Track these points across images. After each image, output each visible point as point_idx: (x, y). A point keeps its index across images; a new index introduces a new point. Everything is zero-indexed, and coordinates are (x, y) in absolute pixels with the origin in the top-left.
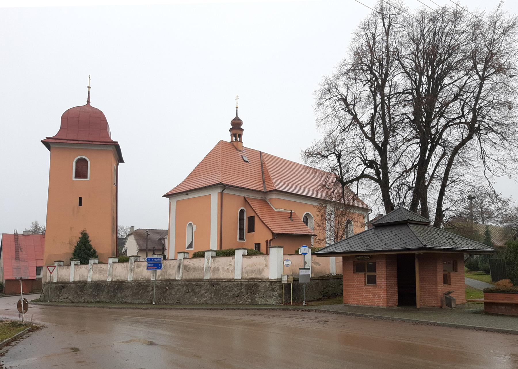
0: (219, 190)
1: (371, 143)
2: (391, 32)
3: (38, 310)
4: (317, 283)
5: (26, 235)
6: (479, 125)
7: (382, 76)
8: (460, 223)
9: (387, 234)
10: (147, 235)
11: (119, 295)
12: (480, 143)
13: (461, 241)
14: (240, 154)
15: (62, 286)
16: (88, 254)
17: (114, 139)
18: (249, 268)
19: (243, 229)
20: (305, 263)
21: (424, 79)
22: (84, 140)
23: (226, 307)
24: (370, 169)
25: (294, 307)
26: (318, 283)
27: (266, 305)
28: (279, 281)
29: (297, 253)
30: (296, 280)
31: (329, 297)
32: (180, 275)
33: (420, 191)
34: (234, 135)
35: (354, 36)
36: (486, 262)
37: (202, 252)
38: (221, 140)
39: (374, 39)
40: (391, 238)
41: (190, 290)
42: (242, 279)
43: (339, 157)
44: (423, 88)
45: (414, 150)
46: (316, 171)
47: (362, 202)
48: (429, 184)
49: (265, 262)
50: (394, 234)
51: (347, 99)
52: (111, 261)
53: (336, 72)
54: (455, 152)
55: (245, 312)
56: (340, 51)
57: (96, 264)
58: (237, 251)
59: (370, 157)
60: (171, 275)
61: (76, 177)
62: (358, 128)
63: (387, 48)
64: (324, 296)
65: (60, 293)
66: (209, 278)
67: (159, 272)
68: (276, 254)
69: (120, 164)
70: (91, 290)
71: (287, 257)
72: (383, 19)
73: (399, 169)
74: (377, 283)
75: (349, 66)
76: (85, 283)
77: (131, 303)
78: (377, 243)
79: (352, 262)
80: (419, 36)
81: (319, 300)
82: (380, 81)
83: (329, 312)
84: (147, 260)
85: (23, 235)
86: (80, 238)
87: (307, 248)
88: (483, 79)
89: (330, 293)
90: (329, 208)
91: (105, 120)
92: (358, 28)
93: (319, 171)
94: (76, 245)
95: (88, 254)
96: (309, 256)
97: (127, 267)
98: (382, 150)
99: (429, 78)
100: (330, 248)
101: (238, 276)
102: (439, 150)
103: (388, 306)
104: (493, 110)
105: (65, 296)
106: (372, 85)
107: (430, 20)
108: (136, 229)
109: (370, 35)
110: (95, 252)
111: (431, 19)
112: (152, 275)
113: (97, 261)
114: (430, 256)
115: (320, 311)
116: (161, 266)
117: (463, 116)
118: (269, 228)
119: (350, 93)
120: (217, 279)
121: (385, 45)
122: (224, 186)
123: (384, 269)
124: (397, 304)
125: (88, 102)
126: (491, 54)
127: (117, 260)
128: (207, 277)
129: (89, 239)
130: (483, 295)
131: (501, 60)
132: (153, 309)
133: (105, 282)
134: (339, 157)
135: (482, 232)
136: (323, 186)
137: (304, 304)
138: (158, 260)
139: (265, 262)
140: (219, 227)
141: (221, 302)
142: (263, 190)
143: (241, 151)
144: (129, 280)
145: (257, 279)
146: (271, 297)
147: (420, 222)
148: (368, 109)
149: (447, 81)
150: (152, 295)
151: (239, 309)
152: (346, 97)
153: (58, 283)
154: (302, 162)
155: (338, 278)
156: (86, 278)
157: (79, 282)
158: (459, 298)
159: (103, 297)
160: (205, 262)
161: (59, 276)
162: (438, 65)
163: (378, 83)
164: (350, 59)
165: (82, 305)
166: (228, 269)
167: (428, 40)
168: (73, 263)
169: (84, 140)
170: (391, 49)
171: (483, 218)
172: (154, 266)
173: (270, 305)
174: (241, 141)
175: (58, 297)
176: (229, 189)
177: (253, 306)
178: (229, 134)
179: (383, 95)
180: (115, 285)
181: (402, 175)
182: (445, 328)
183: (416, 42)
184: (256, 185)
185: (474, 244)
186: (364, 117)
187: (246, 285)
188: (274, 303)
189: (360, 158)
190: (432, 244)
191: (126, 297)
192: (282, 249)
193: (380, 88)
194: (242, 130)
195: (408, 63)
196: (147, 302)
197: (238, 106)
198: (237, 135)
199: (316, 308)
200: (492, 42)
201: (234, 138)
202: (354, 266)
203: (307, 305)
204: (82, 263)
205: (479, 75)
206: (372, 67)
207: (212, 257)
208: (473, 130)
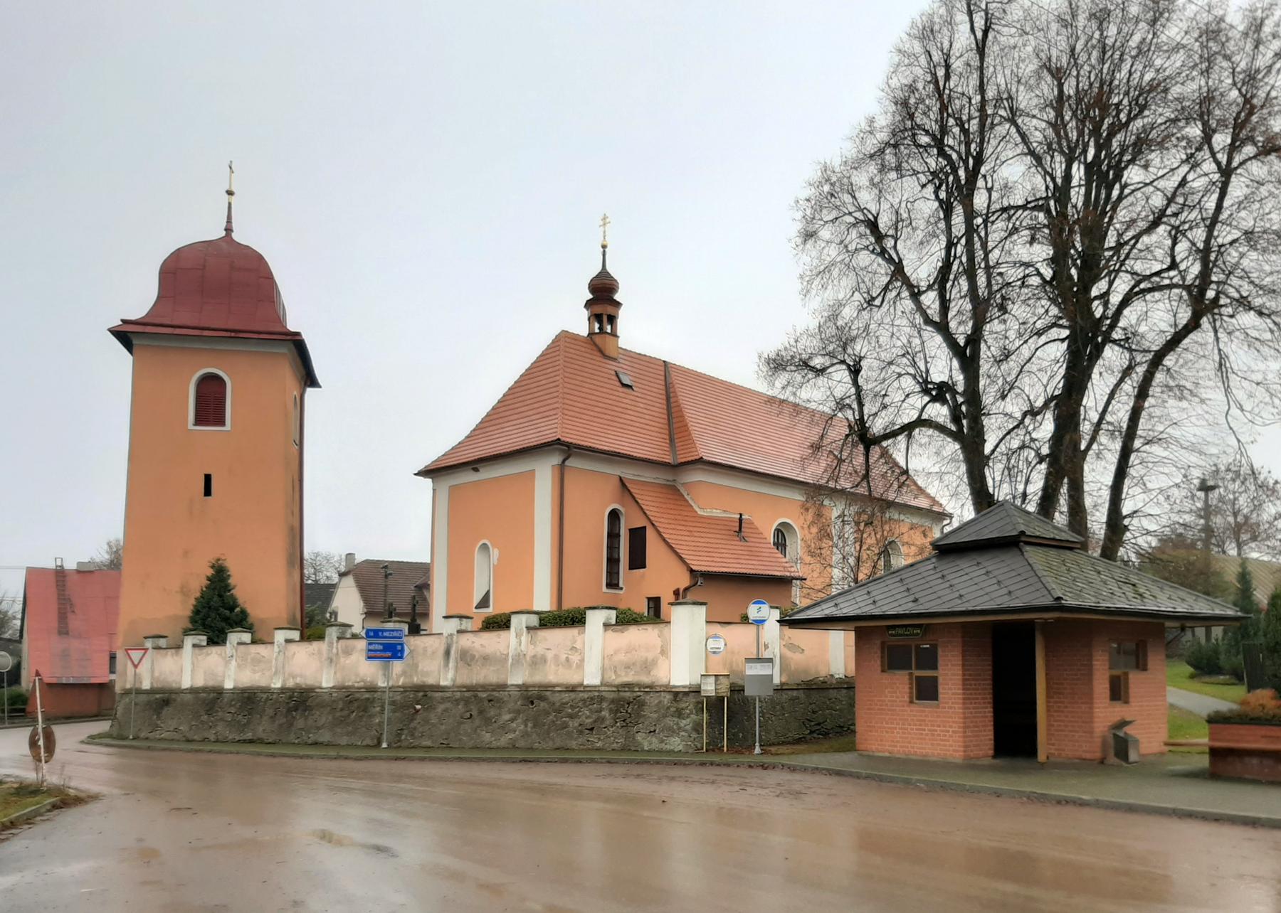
0: (556, 460)
1: (938, 339)
2: (992, 49)
3: (104, 759)
4: (793, 699)
5: (84, 572)
6: (1218, 293)
7: (966, 162)
8: (1182, 553)
9: (967, 571)
10: (386, 576)
11: (300, 723)
12: (1217, 339)
13: (1156, 591)
14: (612, 366)
15: (163, 700)
16: (226, 619)
17: (292, 326)
18: (622, 657)
19: (618, 560)
20: (765, 648)
21: (1078, 172)
22: (217, 327)
23: (563, 756)
24: (938, 405)
25: (731, 759)
26: (798, 698)
27: (661, 752)
28: (696, 691)
29: (745, 620)
30: (737, 690)
31: (826, 734)
32: (451, 674)
33: (1065, 460)
34: (598, 317)
35: (896, 59)
36: (1238, 653)
37: (500, 615)
38: (564, 332)
39: (948, 67)
40: (976, 580)
41: (474, 713)
42: (602, 684)
43: (855, 371)
44: (1077, 196)
45: (1054, 352)
46: (797, 409)
47: (921, 491)
48: (1089, 447)
49: (658, 642)
50: (984, 571)
51: (879, 221)
52: (280, 636)
53: (850, 150)
54: (1157, 361)
55: (605, 769)
56: (854, 95)
58: (589, 614)
59: (938, 376)
61: (199, 421)
62: (905, 294)
63: (982, 89)
64: (812, 732)
65: (158, 718)
66: (520, 682)
67: (397, 666)
68: (687, 623)
69: (309, 391)
71: (718, 629)
72: (970, 13)
73: (1015, 407)
74: (940, 696)
75: (883, 136)
76: (218, 692)
77: (328, 745)
78: (940, 594)
79: (878, 642)
80: (1064, 61)
81: (798, 741)
82: (962, 173)
83: (816, 770)
84: (368, 636)
85: (78, 572)
86: (208, 579)
87: (765, 608)
88: (1226, 172)
89: (829, 725)
90: (835, 510)
91: (269, 277)
92: (905, 37)
93: (806, 409)
94: (198, 595)
95: (226, 619)
96: (772, 629)
97: (320, 652)
98: (967, 355)
99: (1089, 167)
100: (824, 606)
101: (592, 677)
102: (1113, 356)
103: (967, 758)
104: (1253, 255)
105: (171, 723)
106: (940, 185)
107: (1092, 16)
108: (359, 558)
109: (937, 56)
110: (244, 614)
111: (1094, 14)
112: (381, 673)
113: (246, 637)
114: (1075, 628)
115: (793, 769)
116: (402, 651)
117: (1174, 265)
118: (681, 558)
119: (885, 206)
120: (540, 686)
121: (974, 80)
122: (567, 449)
123: (958, 660)
124: (991, 752)
125: (229, 230)
126: (1248, 105)
127: (203, 639)
128: (517, 678)
129: (231, 581)
130: (1206, 729)
131: (1272, 122)
132: (381, 759)
133: (266, 690)
134: (855, 371)
135: (1231, 574)
136: (816, 447)
137: (757, 750)
138: (395, 634)
140: (557, 554)
141: (550, 744)
142: (669, 459)
143: (614, 359)
144: (324, 685)
145: (639, 685)
147: (1054, 539)
148: (933, 250)
149: (1133, 175)
150: (381, 724)
151: (592, 761)
152: (876, 218)
154: (761, 387)
155: (847, 685)
157: (204, 689)
158: (1149, 739)
159: (263, 728)
160: (512, 641)
161: (156, 674)
162: (1112, 133)
163: (957, 178)
164: (885, 117)
165: (209, 748)
166: (567, 660)
167: (1087, 68)
168: (189, 641)
170: (991, 93)
171: (1237, 541)
173: (670, 752)
174: (614, 334)
175: (155, 727)
177: (630, 756)
178: (585, 314)
179: (970, 214)
180: (291, 697)
181: (1022, 422)
182: (1101, 812)
183: (1058, 75)
184: (649, 444)
185: (1190, 599)
186: (922, 268)
187: (613, 701)
188: (681, 747)
189: (914, 377)
190: (1078, 596)
191: (318, 728)
192: (703, 608)
193: (966, 192)
194: (618, 304)
195: (1038, 129)
196: (368, 741)
197: (609, 242)
198: (605, 318)
199: (784, 760)
200: (1251, 78)
201: (597, 326)
202: (882, 652)
203: (764, 752)
204: (213, 642)
205: (1218, 163)
206: (942, 140)
207: (529, 628)
208: (1202, 305)
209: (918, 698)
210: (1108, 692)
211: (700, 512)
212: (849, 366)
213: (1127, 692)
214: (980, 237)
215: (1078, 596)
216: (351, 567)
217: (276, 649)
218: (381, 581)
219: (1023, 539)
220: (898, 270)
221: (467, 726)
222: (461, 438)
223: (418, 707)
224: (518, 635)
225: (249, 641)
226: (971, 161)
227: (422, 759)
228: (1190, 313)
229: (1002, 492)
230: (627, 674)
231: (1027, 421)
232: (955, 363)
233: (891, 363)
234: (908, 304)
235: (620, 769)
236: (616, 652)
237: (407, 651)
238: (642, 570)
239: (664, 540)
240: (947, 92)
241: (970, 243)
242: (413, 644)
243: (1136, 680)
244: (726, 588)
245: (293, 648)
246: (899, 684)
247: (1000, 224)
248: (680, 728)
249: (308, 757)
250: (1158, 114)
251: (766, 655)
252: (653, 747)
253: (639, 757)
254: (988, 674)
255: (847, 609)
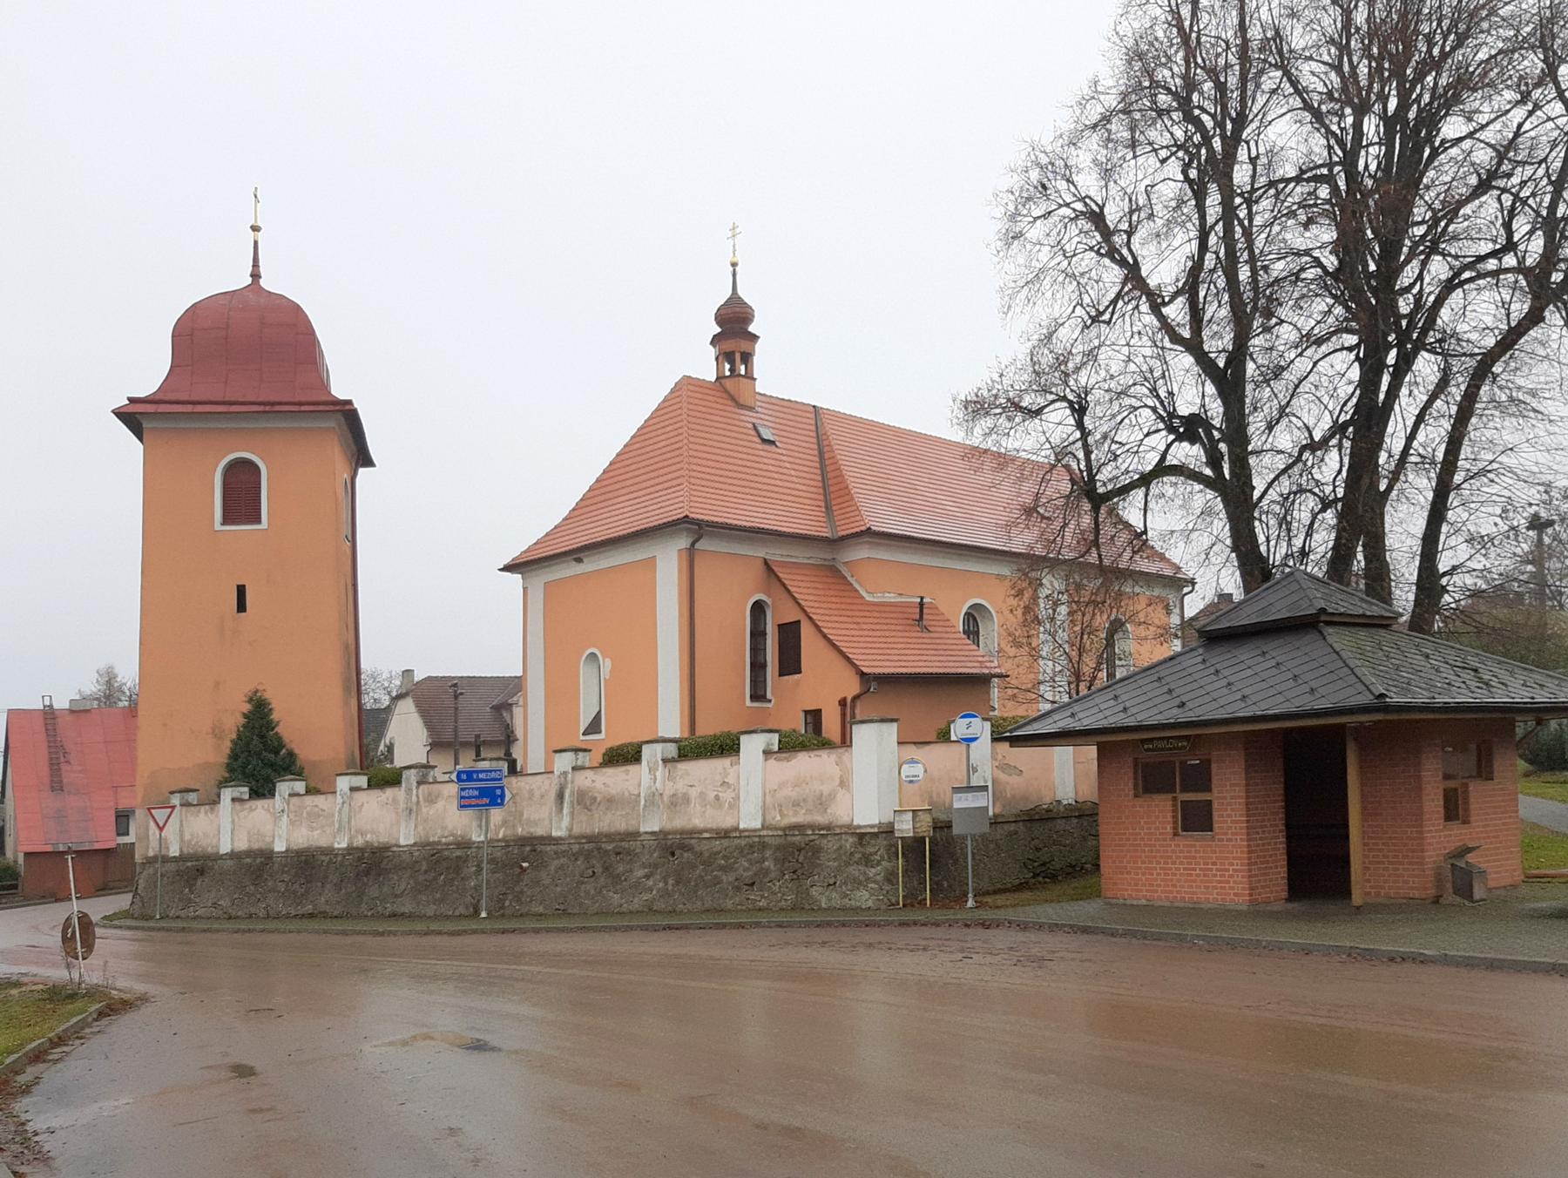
0: (683, 542)
1: (1188, 360)
8: (1502, 612)
10: (456, 697)
11: (373, 891)
13: (1506, 677)
15: (196, 868)
17: (339, 391)
18: (788, 792)
20: (972, 771)
21: (1371, 126)
22: (246, 400)
23: (717, 920)
24: (1185, 444)
25: (938, 915)
26: (1016, 833)
27: (843, 909)
28: (887, 831)
29: (944, 737)
30: (942, 826)
31: (1054, 877)
32: (566, 822)
33: (1360, 511)
34: (726, 356)
41: (599, 870)
42: (763, 827)
44: (1370, 159)
46: (1003, 460)
47: (1162, 557)
48: (1390, 488)
49: (837, 772)
51: (1106, 211)
52: (343, 783)
53: (1067, 125)
57: (298, 795)
60: (535, 823)
61: (225, 521)
66: (656, 829)
67: (496, 815)
69: (361, 470)
70: (286, 878)
71: (912, 752)
73: (1286, 438)
74: (1215, 826)
75: (1112, 101)
76: (267, 855)
77: (410, 917)
78: (1215, 695)
79: (1130, 760)
81: (1019, 888)
82: (1217, 144)
83: (1054, 928)
85: (71, 711)
86: (245, 716)
90: (1051, 583)
94: (234, 736)
96: (983, 748)
97: (395, 800)
98: (1228, 379)
99: (1389, 122)
100: (1056, 717)
101: (750, 819)
102: (1426, 367)
106: (1191, 161)
108: (419, 676)
112: (475, 824)
113: (300, 786)
114: (1397, 732)
115: (1024, 927)
116: (503, 796)
117: (1510, 246)
120: (682, 832)
122: (697, 528)
124: (1285, 894)
125: (256, 276)
128: (651, 824)
129: (275, 716)
133: (329, 851)
136: (1030, 511)
137: (970, 903)
138: (493, 775)
139: (837, 772)
142: (826, 533)
143: (751, 409)
144: (402, 842)
145: (812, 827)
146: (860, 883)
147: (1363, 616)
148: (1176, 243)
150: (477, 888)
151: (758, 925)
152: (1102, 208)
153: (182, 858)
154: (957, 435)
155: (1084, 815)
156: (268, 839)
157: (249, 853)
158: (1498, 866)
159: (325, 898)
161: (187, 837)
162: (1420, 77)
163: (1210, 149)
164: (1111, 75)
168: (227, 794)
169: (246, 400)
170: (1255, 33)
172: (481, 796)
173: (857, 910)
174: (749, 376)
176: (712, 535)
177: (802, 917)
178: (712, 352)
180: (360, 859)
182: (1453, 970)
184: (806, 521)
185: (1551, 684)
186: (1164, 270)
187: (778, 848)
188: (870, 904)
189: (1154, 409)
190: (1406, 688)
193: (1220, 169)
194: (754, 338)
195: (1315, 76)
196: (461, 910)
197: (738, 259)
198: (738, 356)
199: (1010, 914)
201: (727, 366)
203: (980, 905)
206: (1189, 99)
207: (665, 761)
209: (1184, 830)
210: (1442, 810)
211: (868, 598)
212: (1071, 403)
213: (1467, 810)
214: (1241, 223)
215: (1405, 691)
216: (409, 686)
217: (339, 800)
218: (449, 701)
219: (1323, 618)
220: (1133, 273)
221: (590, 887)
222: (558, 521)
223: (525, 865)
224: (652, 770)
225: (303, 791)
226: (1229, 126)
227: (537, 931)
228: (1526, 307)
229: (1276, 552)
230: (796, 814)
231: (1306, 455)
232: (1210, 389)
233: (1123, 393)
234: (1151, 319)
235: (800, 934)
236: (782, 785)
237: (508, 795)
238: (796, 677)
239: (825, 636)
240: (1194, 35)
241: (1228, 230)
242: (513, 785)
243: (1478, 793)
244: (924, 696)
245: (361, 797)
246: (1160, 811)
247: (1265, 204)
248: (868, 879)
249: (390, 933)
250: (1484, 47)
251: (976, 781)
252: (833, 903)
253: (819, 918)
254: (1279, 789)
255: (1088, 718)
